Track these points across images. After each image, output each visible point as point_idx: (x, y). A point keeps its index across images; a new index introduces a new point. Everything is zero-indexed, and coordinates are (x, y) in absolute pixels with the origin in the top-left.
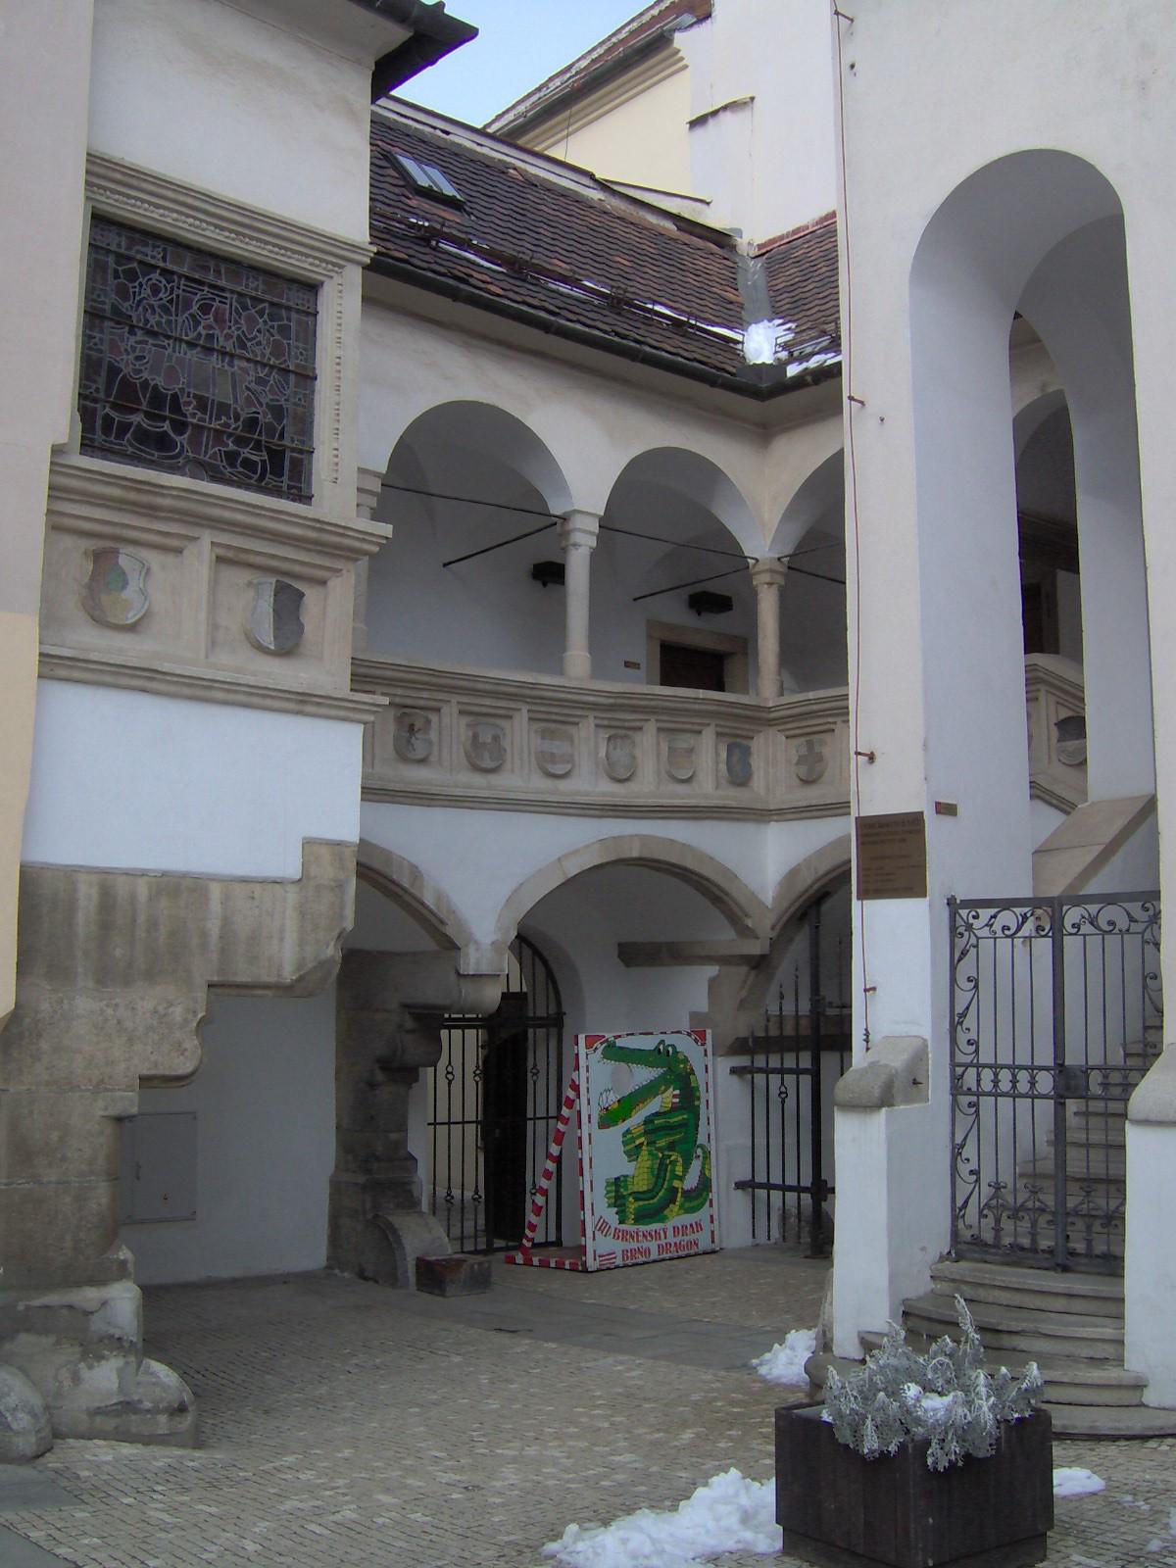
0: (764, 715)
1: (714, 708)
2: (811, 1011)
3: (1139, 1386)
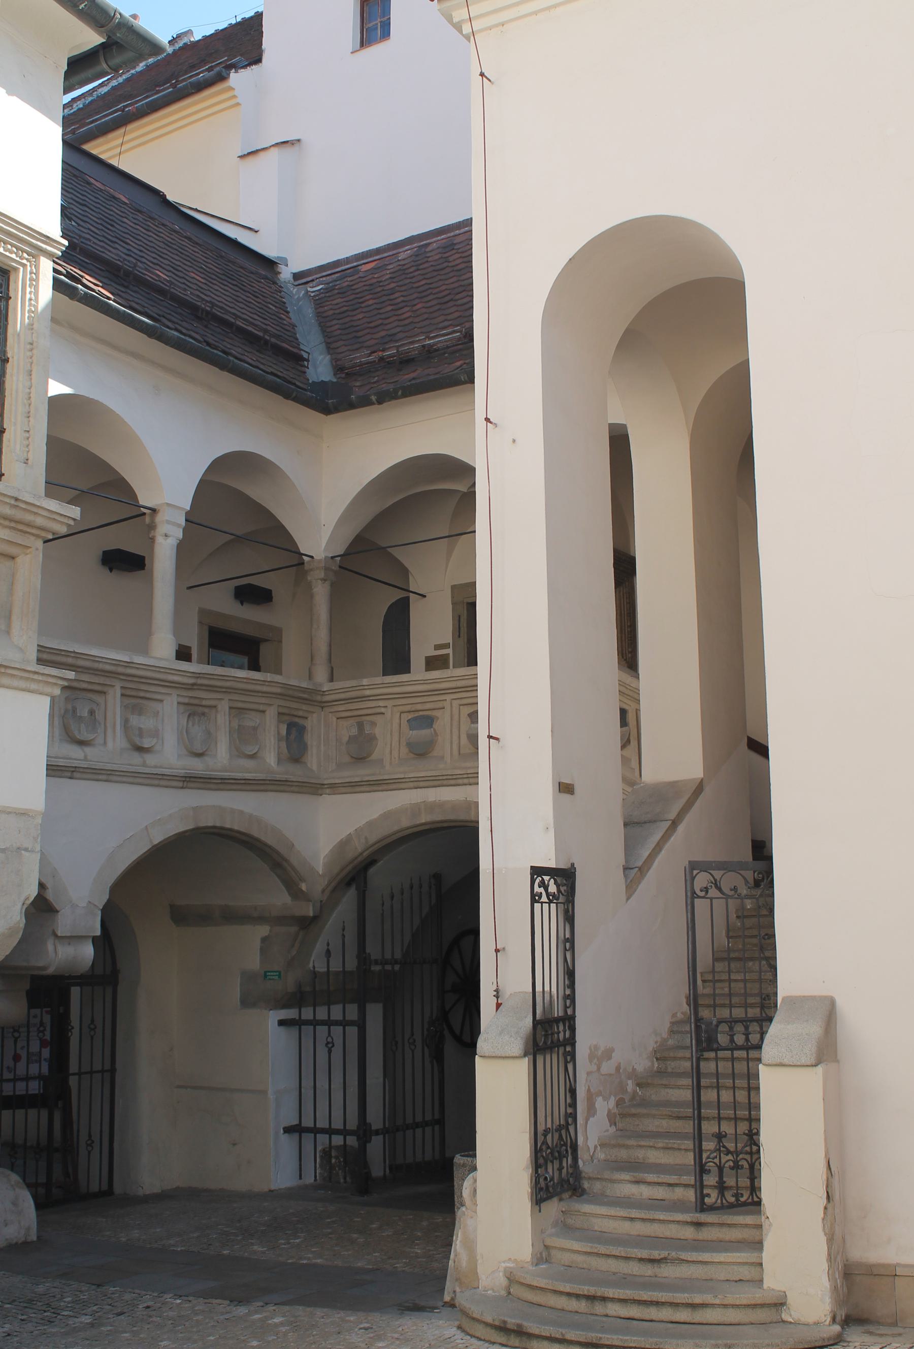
0: (319, 698)
1: (279, 690)
3: (779, 1304)
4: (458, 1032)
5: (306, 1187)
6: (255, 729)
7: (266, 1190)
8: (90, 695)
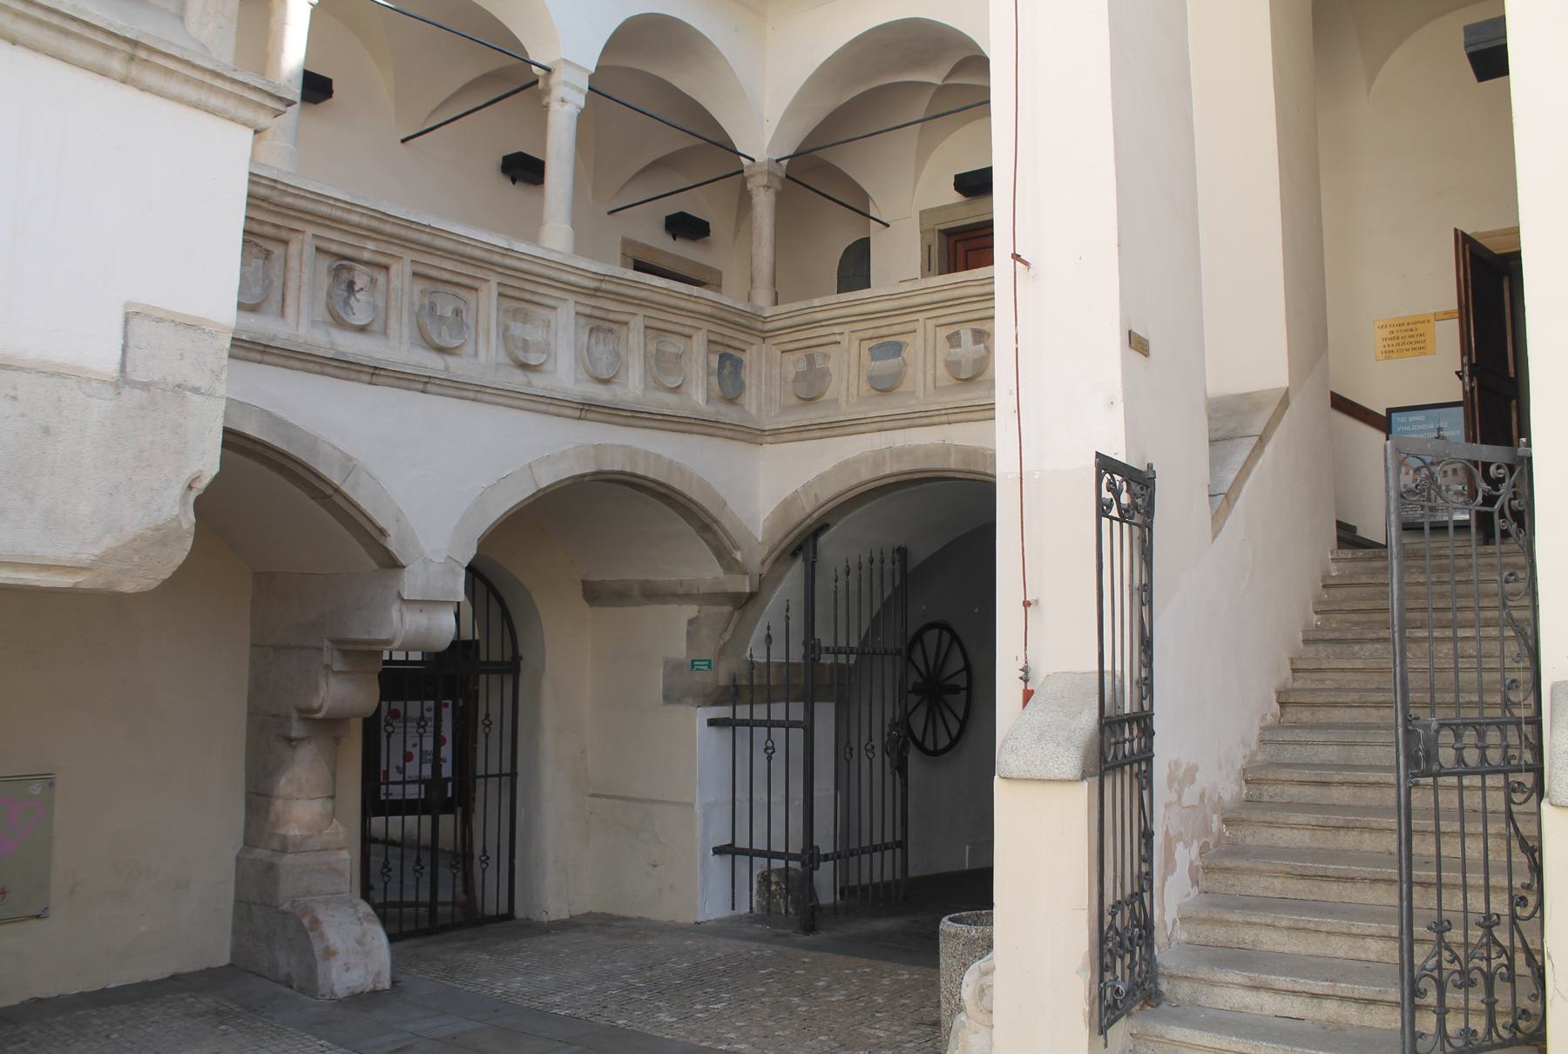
0: (759, 326)
2: (805, 657)
4: (920, 738)
5: (740, 918)
6: (679, 357)
7: (692, 921)
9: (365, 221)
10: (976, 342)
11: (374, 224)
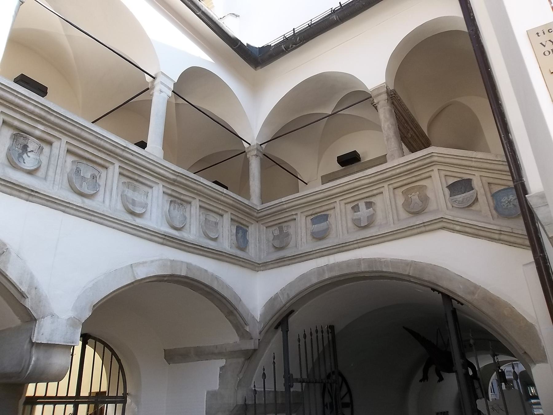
0: (255, 214)
1: (231, 202)
8: (95, 166)
9: (37, 110)
10: (368, 208)
11: (43, 113)
